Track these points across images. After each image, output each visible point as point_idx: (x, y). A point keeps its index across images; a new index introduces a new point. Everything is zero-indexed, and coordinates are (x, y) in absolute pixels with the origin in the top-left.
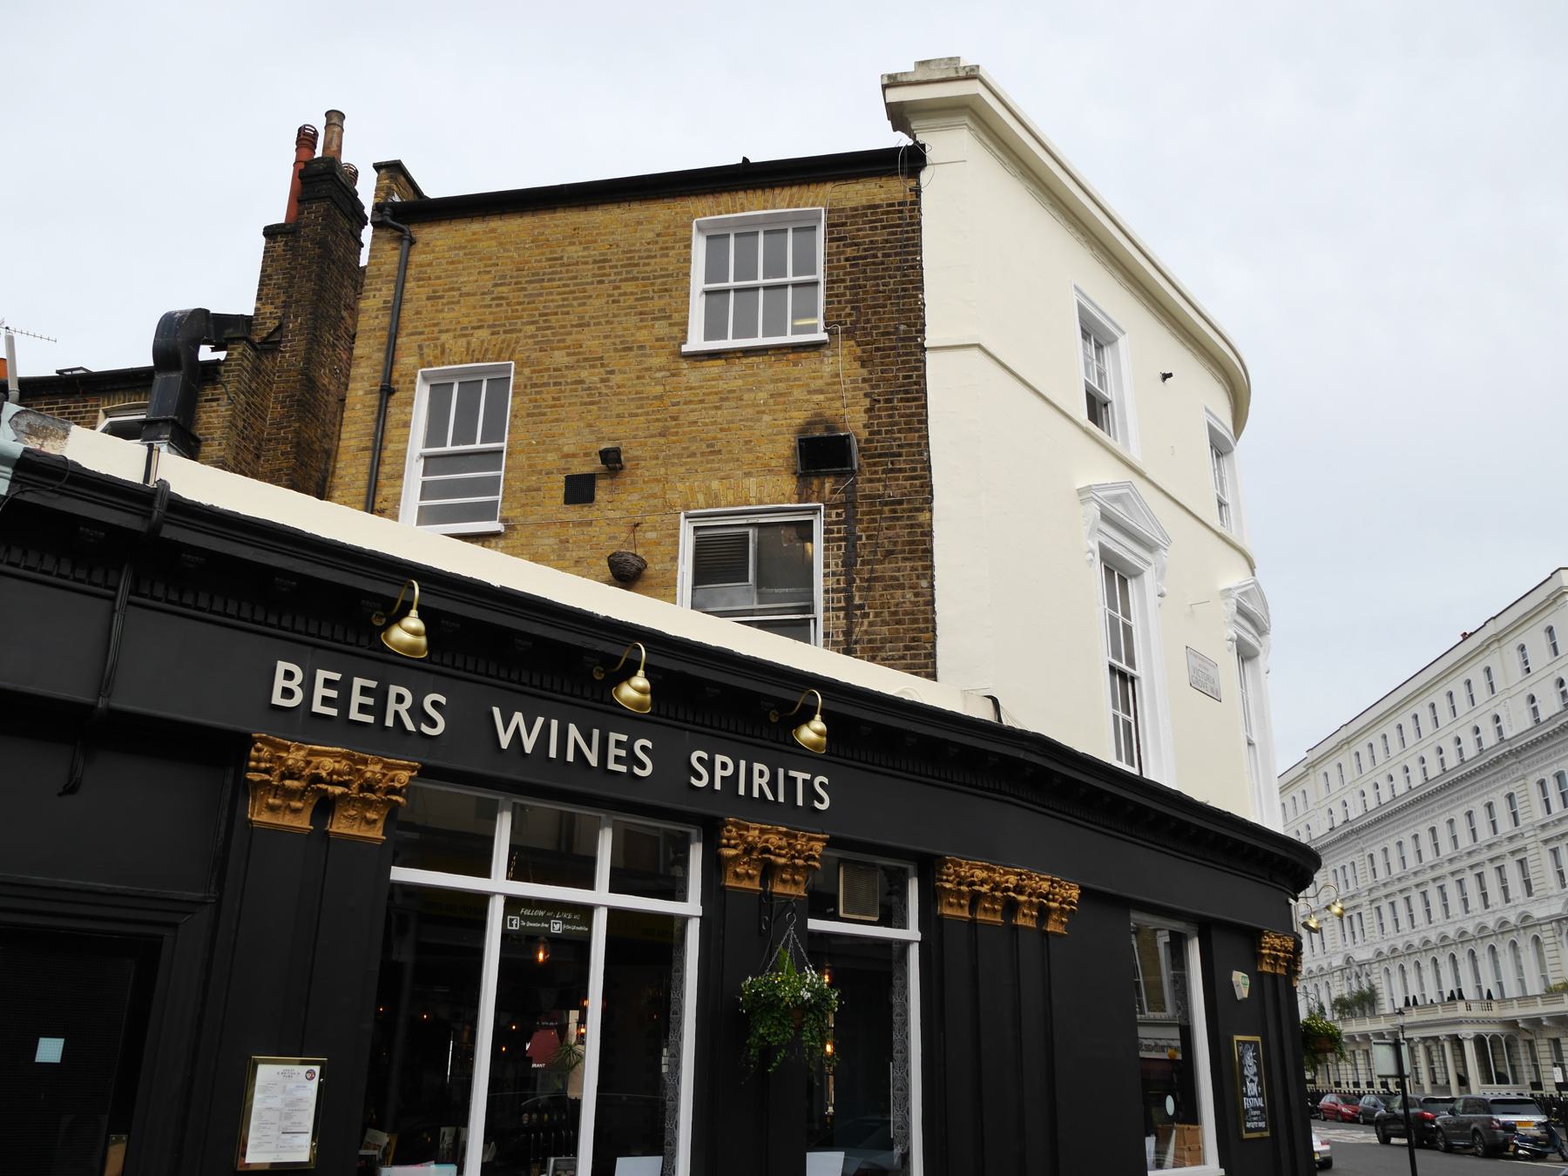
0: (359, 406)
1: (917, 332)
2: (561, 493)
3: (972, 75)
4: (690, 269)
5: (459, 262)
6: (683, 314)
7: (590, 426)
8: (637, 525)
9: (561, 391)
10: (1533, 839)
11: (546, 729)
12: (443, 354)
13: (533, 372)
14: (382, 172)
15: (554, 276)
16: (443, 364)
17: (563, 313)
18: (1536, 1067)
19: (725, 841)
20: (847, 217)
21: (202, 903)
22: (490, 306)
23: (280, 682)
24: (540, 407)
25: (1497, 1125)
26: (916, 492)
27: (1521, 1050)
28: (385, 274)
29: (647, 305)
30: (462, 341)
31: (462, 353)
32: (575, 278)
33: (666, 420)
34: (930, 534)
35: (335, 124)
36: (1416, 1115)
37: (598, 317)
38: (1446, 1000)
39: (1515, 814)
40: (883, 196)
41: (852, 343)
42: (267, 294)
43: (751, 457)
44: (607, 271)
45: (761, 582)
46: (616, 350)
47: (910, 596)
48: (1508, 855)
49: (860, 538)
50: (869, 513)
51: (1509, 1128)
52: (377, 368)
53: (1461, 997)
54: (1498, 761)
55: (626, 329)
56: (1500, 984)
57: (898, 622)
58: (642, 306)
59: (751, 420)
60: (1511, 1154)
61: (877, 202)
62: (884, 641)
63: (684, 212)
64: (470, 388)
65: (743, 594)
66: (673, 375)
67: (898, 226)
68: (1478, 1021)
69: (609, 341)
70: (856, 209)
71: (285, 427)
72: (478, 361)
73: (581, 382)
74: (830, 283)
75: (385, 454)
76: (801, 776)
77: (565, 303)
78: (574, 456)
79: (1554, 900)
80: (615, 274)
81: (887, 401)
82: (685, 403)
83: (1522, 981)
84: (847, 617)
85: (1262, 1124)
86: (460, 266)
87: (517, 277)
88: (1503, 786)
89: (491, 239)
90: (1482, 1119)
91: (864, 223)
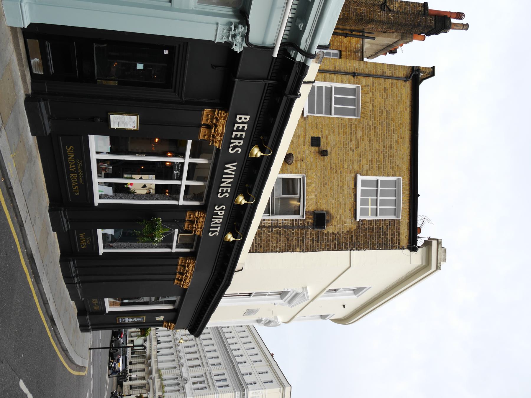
0: (350, 65)
1: (357, 248)
2: (315, 136)
3: (438, 268)
4: (385, 176)
5: (396, 98)
6: (370, 174)
7: (336, 144)
8: (303, 161)
9: (348, 134)
10: (206, 370)
11: (232, 174)
12: (365, 93)
13: (356, 125)
14: (432, 69)
15: (388, 131)
16: (362, 94)
17: (375, 134)
18: (136, 364)
19: (200, 213)
20: (397, 226)
21: (181, 98)
22: (380, 109)
23: (243, 117)
24: (344, 128)
25: (119, 357)
26: (306, 247)
27: (142, 360)
28: (395, 72)
29: (374, 162)
30: (369, 101)
31: (365, 100)
32: (386, 138)
33: (336, 169)
34: (293, 251)
35: (463, 27)
36: (122, 332)
37: (372, 146)
38: (157, 338)
39: (215, 365)
40: (402, 238)
41: (355, 228)
42: (402, 5)
43: (321, 197)
44: (388, 149)
45: (282, 198)
46: (360, 152)
47: (275, 245)
48: (202, 362)
49: (293, 230)
50: (301, 233)
51: (118, 361)
52: (363, 70)
53: (158, 343)
54: (232, 362)
55: (367, 156)
56: (162, 355)
57: (267, 242)
58: (374, 161)
59: (333, 197)
60: (110, 360)
61: (400, 236)
62: (261, 237)
63: (404, 174)
64: (353, 102)
65: (279, 193)
66: (350, 171)
67: (392, 243)
68: (150, 348)
69: (364, 150)
70: (399, 229)
71: (353, 14)
72: (361, 106)
73: (351, 141)
74: (375, 221)
75: (333, 75)
76: (218, 229)
77: (378, 135)
78: (327, 139)
79: (187, 374)
80: (386, 152)
81: (335, 239)
82: (341, 175)
83: (163, 362)
84: (269, 226)
85: (120, 322)
86: (395, 98)
87: (389, 118)
88: (224, 362)
89: (403, 109)
90: (121, 352)
91: (394, 232)
